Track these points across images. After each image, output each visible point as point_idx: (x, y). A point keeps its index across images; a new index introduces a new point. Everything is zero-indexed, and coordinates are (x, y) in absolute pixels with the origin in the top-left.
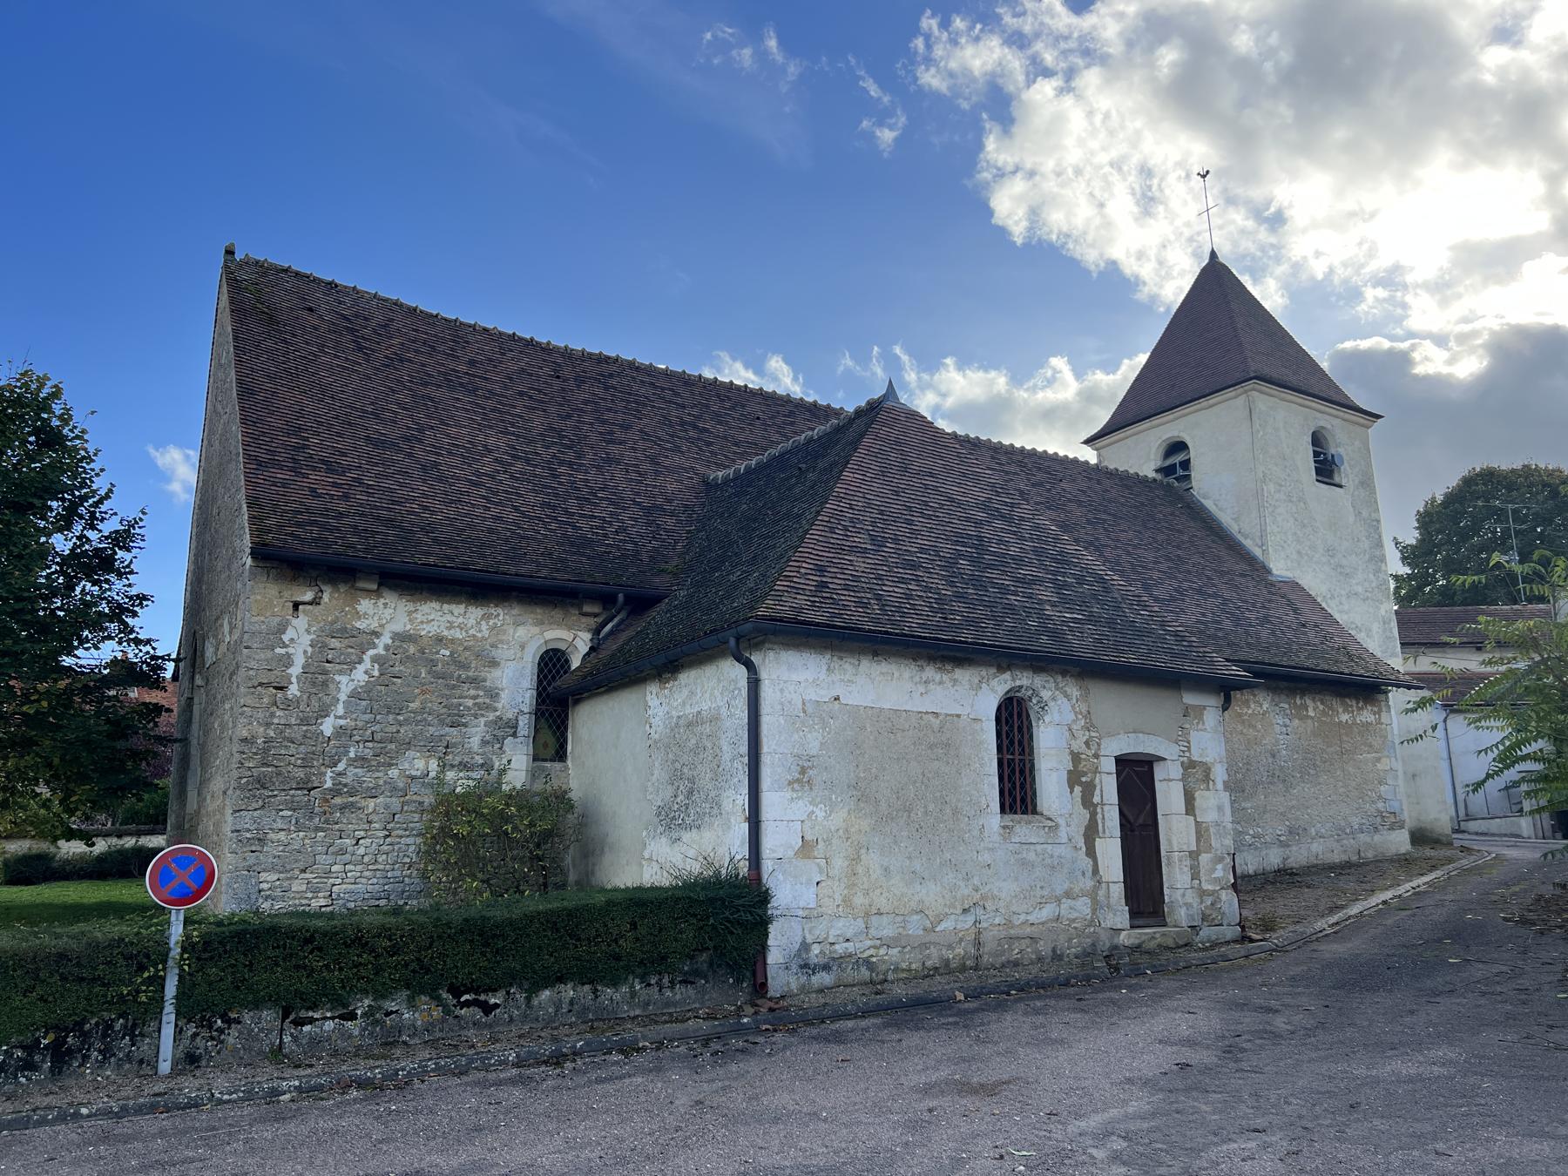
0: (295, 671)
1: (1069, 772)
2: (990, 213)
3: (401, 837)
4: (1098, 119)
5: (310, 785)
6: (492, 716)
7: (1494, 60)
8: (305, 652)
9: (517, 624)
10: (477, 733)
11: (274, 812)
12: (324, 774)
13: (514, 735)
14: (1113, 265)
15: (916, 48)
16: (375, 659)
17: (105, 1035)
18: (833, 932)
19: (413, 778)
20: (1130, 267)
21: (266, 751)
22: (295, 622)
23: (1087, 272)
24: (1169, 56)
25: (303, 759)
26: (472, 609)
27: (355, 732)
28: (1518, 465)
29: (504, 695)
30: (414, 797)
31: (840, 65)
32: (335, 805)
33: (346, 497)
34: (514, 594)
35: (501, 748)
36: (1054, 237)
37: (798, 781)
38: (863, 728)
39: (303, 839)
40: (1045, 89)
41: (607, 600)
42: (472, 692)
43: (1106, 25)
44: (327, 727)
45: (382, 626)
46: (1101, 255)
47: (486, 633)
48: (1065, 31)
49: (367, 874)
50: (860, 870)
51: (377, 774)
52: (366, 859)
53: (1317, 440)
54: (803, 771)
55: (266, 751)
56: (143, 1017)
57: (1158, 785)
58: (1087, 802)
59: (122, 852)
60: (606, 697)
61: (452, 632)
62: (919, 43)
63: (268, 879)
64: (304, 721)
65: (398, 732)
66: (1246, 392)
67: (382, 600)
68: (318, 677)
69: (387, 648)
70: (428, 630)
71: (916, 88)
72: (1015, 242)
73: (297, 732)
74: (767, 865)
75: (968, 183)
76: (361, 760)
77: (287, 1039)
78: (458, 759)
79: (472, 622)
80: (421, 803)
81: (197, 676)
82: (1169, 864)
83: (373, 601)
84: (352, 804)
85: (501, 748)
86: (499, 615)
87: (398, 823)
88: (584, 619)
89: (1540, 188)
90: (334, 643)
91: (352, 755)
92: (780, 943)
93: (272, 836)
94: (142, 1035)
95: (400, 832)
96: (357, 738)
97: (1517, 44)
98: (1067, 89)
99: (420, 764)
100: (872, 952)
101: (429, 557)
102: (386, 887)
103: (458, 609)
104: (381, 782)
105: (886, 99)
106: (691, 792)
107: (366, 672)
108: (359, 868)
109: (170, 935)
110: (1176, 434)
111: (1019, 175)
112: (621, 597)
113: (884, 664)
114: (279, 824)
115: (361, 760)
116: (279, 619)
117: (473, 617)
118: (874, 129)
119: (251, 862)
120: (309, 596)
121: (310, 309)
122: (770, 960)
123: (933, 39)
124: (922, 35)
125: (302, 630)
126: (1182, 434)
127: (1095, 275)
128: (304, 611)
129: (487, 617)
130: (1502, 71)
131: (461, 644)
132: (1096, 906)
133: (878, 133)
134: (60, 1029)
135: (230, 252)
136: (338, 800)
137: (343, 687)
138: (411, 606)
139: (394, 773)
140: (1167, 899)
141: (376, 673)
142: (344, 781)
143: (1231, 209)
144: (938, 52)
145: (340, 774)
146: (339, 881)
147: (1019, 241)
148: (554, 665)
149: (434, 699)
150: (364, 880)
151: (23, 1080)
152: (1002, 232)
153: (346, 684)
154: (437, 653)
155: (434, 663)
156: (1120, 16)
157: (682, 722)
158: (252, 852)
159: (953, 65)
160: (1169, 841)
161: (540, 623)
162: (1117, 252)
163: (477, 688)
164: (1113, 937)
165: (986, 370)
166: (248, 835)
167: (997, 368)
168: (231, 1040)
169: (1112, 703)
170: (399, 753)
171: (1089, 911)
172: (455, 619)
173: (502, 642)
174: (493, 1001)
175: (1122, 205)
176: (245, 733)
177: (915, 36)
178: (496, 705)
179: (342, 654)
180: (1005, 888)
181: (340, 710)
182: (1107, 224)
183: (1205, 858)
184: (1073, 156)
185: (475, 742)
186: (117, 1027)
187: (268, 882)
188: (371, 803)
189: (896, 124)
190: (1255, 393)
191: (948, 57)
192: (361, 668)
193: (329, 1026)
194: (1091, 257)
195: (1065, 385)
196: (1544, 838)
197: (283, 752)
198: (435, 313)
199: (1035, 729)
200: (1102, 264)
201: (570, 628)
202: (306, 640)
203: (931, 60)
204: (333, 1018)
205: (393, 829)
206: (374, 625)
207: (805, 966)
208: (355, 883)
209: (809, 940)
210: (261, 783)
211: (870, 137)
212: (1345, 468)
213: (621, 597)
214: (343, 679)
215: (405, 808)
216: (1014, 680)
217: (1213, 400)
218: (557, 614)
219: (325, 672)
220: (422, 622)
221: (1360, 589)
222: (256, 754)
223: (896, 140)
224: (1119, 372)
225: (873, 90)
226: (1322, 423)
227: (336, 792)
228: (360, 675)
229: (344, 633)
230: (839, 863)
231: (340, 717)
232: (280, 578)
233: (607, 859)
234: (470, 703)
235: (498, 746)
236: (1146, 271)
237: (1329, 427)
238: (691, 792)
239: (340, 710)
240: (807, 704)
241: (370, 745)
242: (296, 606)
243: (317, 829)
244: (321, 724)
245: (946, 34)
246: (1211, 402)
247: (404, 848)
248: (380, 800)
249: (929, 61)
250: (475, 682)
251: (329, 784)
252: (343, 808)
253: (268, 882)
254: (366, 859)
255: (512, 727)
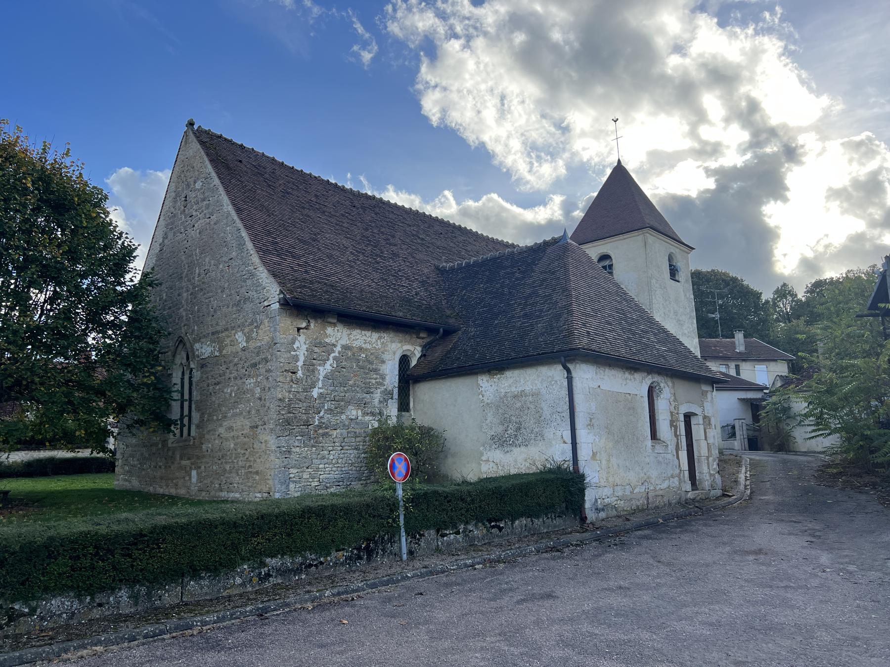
0: (300, 363)
1: (671, 421)
2: (419, 107)
3: (347, 450)
4: (482, 67)
5: (309, 424)
6: (383, 388)
7: (674, 62)
8: (304, 354)
9: (392, 342)
10: (377, 396)
11: (294, 438)
12: (315, 417)
13: (392, 398)
14: (483, 145)
15: (387, 10)
16: (335, 358)
17: (382, 543)
18: (604, 494)
19: (352, 420)
20: (490, 146)
21: (289, 405)
22: (299, 338)
23: (469, 146)
24: (520, 38)
25: (305, 410)
26: (374, 334)
27: (327, 396)
28: (709, 270)
29: (387, 378)
30: (353, 430)
31: (343, 14)
32: (320, 434)
33: (306, 272)
34: (391, 326)
35: (387, 405)
36: (454, 125)
37: (590, 425)
38: (608, 401)
39: (307, 452)
40: (455, 45)
41: (431, 331)
42: (375, 376)
43: (489, 15)
44: (315, 393)
45: (337, 341)
46: (477, 138)
47: (380, 346)
48: (468, 15)
49: (334, 469)
50: (610, 465)
51: (337, 418)
52: (334, 461)
53: (670, 258)
54: (591, 421)
55: (289, 405)
56: (393, 532)
57: (692, 426)
58: (676, 435)
59: (39, 461)
60: (444, 380)
61: (366, 345)
62: (389, 8)
63: (293, 472)
64: (305, 390)
65: (345, 396)
66: (643, 233)
67: (336, 328)
68: (310, 367)
69: (339, 353)
70: (356, 344)
71: (385, 32)
72: (432, 125)
73: (302, 396)
74: (581, 464)
75: (411, 90)
76: (330, 411)
77: (440, 543)
78: (370, 410)
79: (374, 340)
80: (355, 433)
81: (191, 363)
82: (699, 462)
83: (333, 328)
84: (327, 433)
85: (387, 405)
86: (384, 337)
87: (346, 443)
88: (418, 340)
89: (686, 128)
90: (316, 350)
91: (326, 408)
92: (590, 496)
93: (293, 449)
94: (394, 542)
95: (347, 447)
96: (328, 399)
97: (684, 55)
98: (467, 46)
99: (354, 412)
100: (615, 503)
101: (361, 307)
102: (342, 476)
103: (368, 333)
104: (339, 422)
105: (367, 35)
106: (519, 429)
107: (331, 365)
108: (331, 466)
109: (399, 495)
110: (605, 251)
111: (438, 89)
112: (441, 330)
113: (613, 371)
114: (297, 444)
115: (330, 411)
116: (292, 336)
117: (374, 337)
118: (360, 51)
119: (286, 463)
120: (304, 325)
121: (240, 161)
122: (586, 507)
123: (398, 7)
124: (391, 3)
125: (302, 343)
126: (609, 252)
127: (473, 148)
128: (303, 333)
129: (380, 338)
130: (675, 68)
131: (370, 352)
132: (680, 481)
133: (362, 54)
134: (368, 540)
135: (191, 124)
136: (321, 431)
137: (321, 372)
138: (349, 332)
139: (344, 417)
140: (697, 478)
141: (335, 366)
142: (323, 421)
143: (544, 121)
144: (399, 14)
145: (321, 418)
146: (322, 473)
147: (435, 124)
148: (404, 363)
149: (359, 379)
150: (333, 472)
151: (358, 564)
152: (426, 119)
153: (324, 370)
154: (360, 356)
155: (358, 361)
156: (497, 12)
157: (509, 395)
158: (286, 458)
159: (408, 23)
160: (699, 452)
161: (401, 342)
162: (486, 138)
163: (377, 374)
164: (686, 495)
165: (410, 194)
166: (284, 449)
167: (415, 193)
168: (422, 544)
169: (683, 389)
170: (346, 407)
171: (678, 483)
172: (367, 339)
173: (386, 351)
174: (501, 525)
175: (490, 114)
176: (280, 396)
177: (387, 4)
178: (384, 383)
179: (320, 355)
180: (654, 473)
181: (320, 384)
182: (481, 121)
183: (711, 459)
184: (469, 84)
185: (376, 401)
186: (386, 538)
187: (293, 474)
188: (335, 433)
189: (372, 49)
190: (648, 235)
191: (405, 17)
192: (329, 363)
193: (452, 536)
194: (471, 138)
195: (450, 206)
196: (745, 450)
197: (297, 406)
198: (291, 166)
199: (655, 401)
200: (477, 142)
201: (413, 345)
202: (304, 347)
203: (395, 18)
204: (453, 534)
205: (345, 446)
206: (333, 341)
207: (597, 509)
208: (329, 474)
209: (597, 498)
210: (288, 422)
211: (357, 56)
212: (681, 273)
213: (441, 330)
214: (321, 368)
215: (349, 435)
216: (652, 378)
217: (626, 236)
218: (408, 337)
219: (313, 365)
220: (354, 340)
221: (686, 332)
222: (285, 407)
223: (372, 59)
224: (481, 202)
225: (360, 29)
226: (672, 251)
227: (320, 427)
228: (328, 366)
229: (320, 344)
230: (604, 462)
231: (320, 388)
232: (291, 315)
233: (450, 460)
234: (374, 381)
235: (386, 403)
236: (498, 149)
237: (674, 252)
238: (519, 429)
239: (320, 384)
240: (591, 390)
241: (333, 402)
242: (299, 329)
243: (313, 446)
244: (312, 392)
245: (405, 5)
246: (625, 237)
247: (349, 456)
248: (338, 431)
249: (394, 19)
250: (376, 371)
251: (317, 423)
252: (324, 435)
253: (293, 474)
254: (334, 461)
255: (391, 393)
